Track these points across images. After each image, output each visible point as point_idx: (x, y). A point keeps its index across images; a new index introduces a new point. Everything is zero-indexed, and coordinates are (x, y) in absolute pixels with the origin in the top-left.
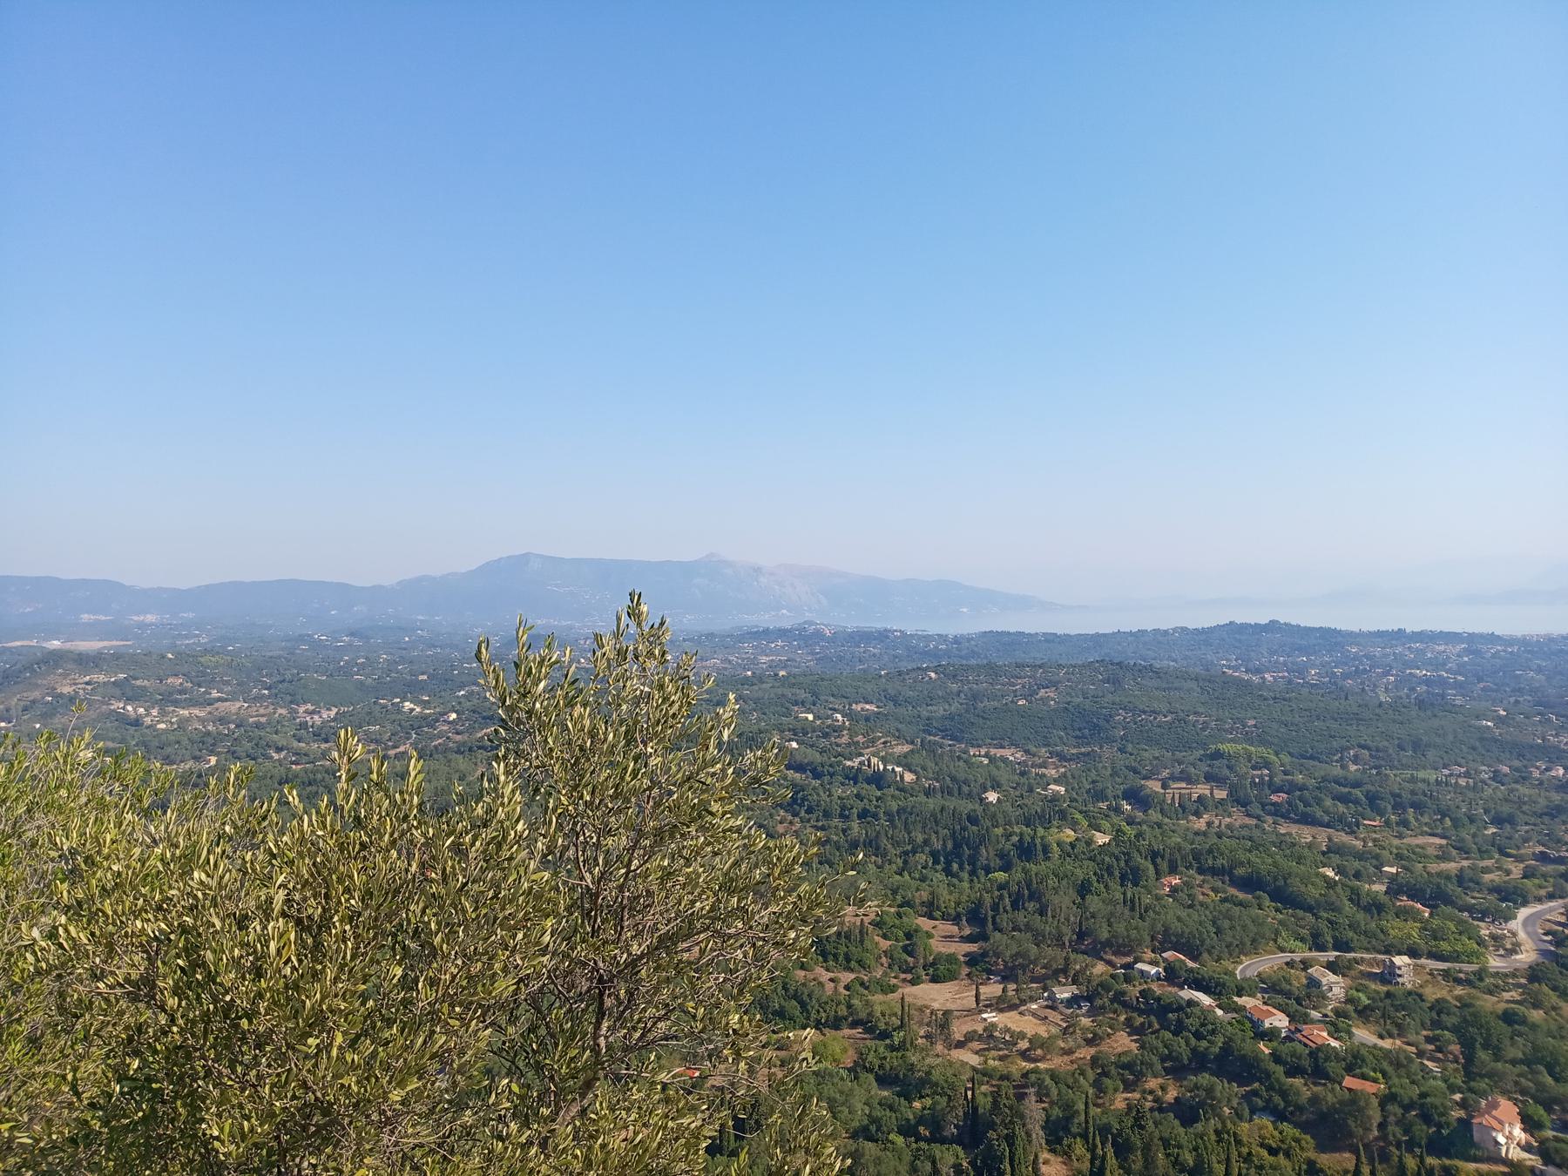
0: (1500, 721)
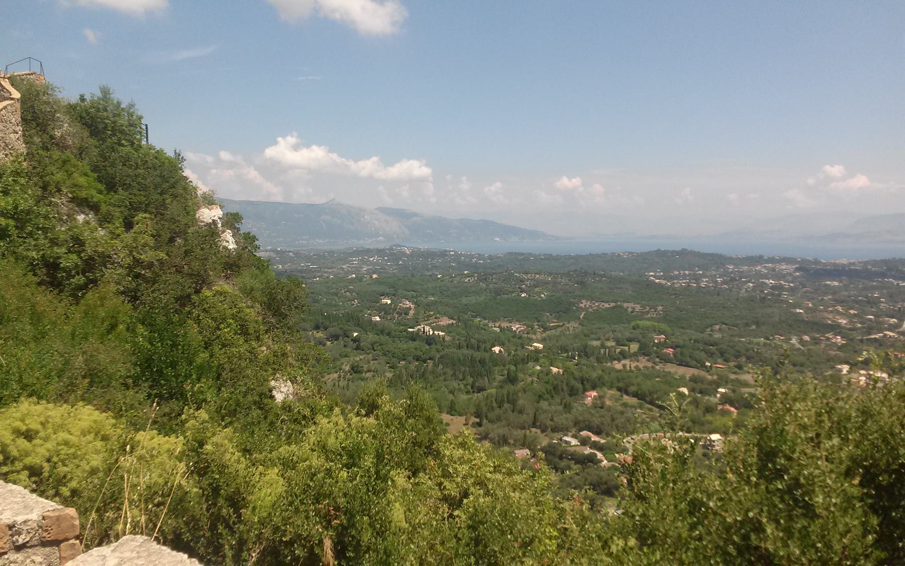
0: (807, 309)
